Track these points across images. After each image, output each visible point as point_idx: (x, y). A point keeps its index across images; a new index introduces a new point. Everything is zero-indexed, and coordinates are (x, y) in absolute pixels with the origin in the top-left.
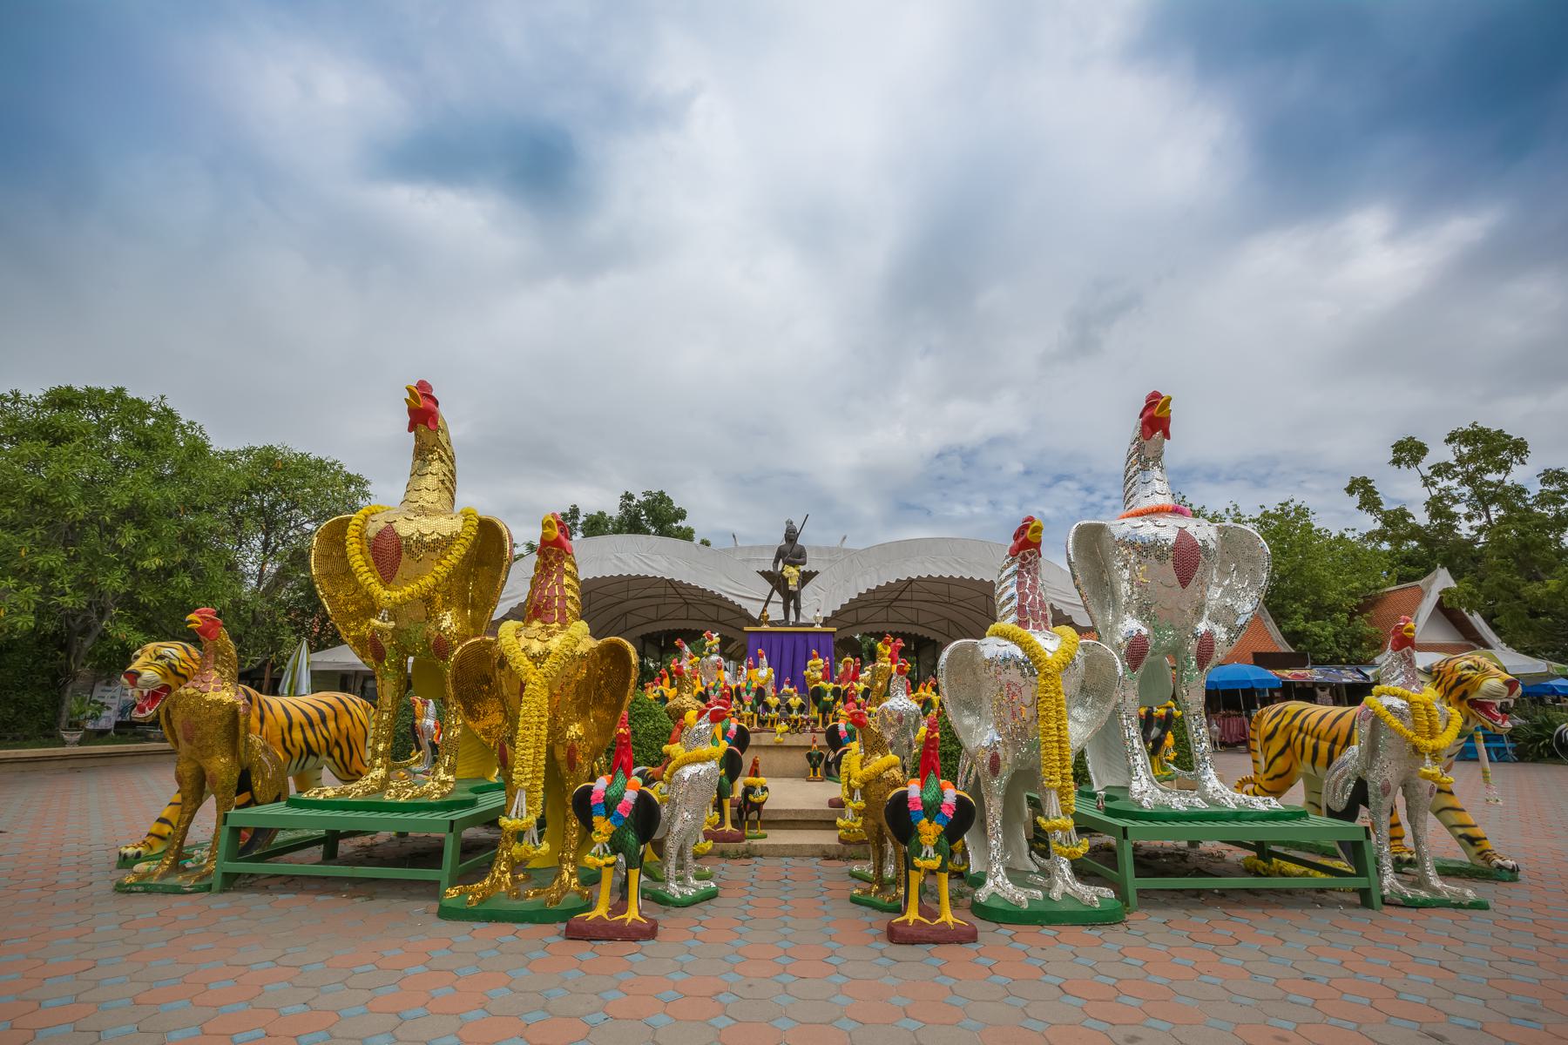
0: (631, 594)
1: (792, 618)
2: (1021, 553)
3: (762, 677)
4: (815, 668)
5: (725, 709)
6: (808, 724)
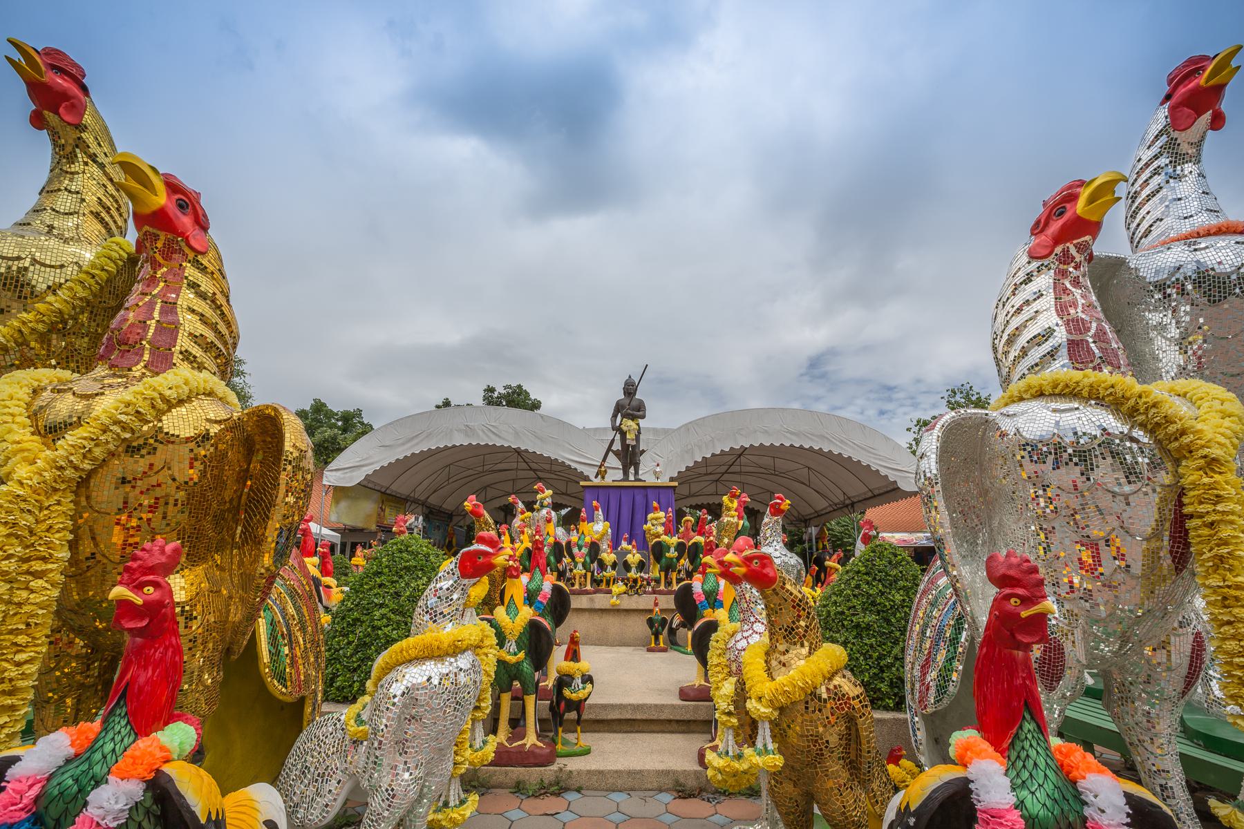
0: (486, 468)
1: (632, 478)
2: (1058, 250)
3: (597, 532)
4: (656, 523)
5: (490, 550)
6: (649, 584)
